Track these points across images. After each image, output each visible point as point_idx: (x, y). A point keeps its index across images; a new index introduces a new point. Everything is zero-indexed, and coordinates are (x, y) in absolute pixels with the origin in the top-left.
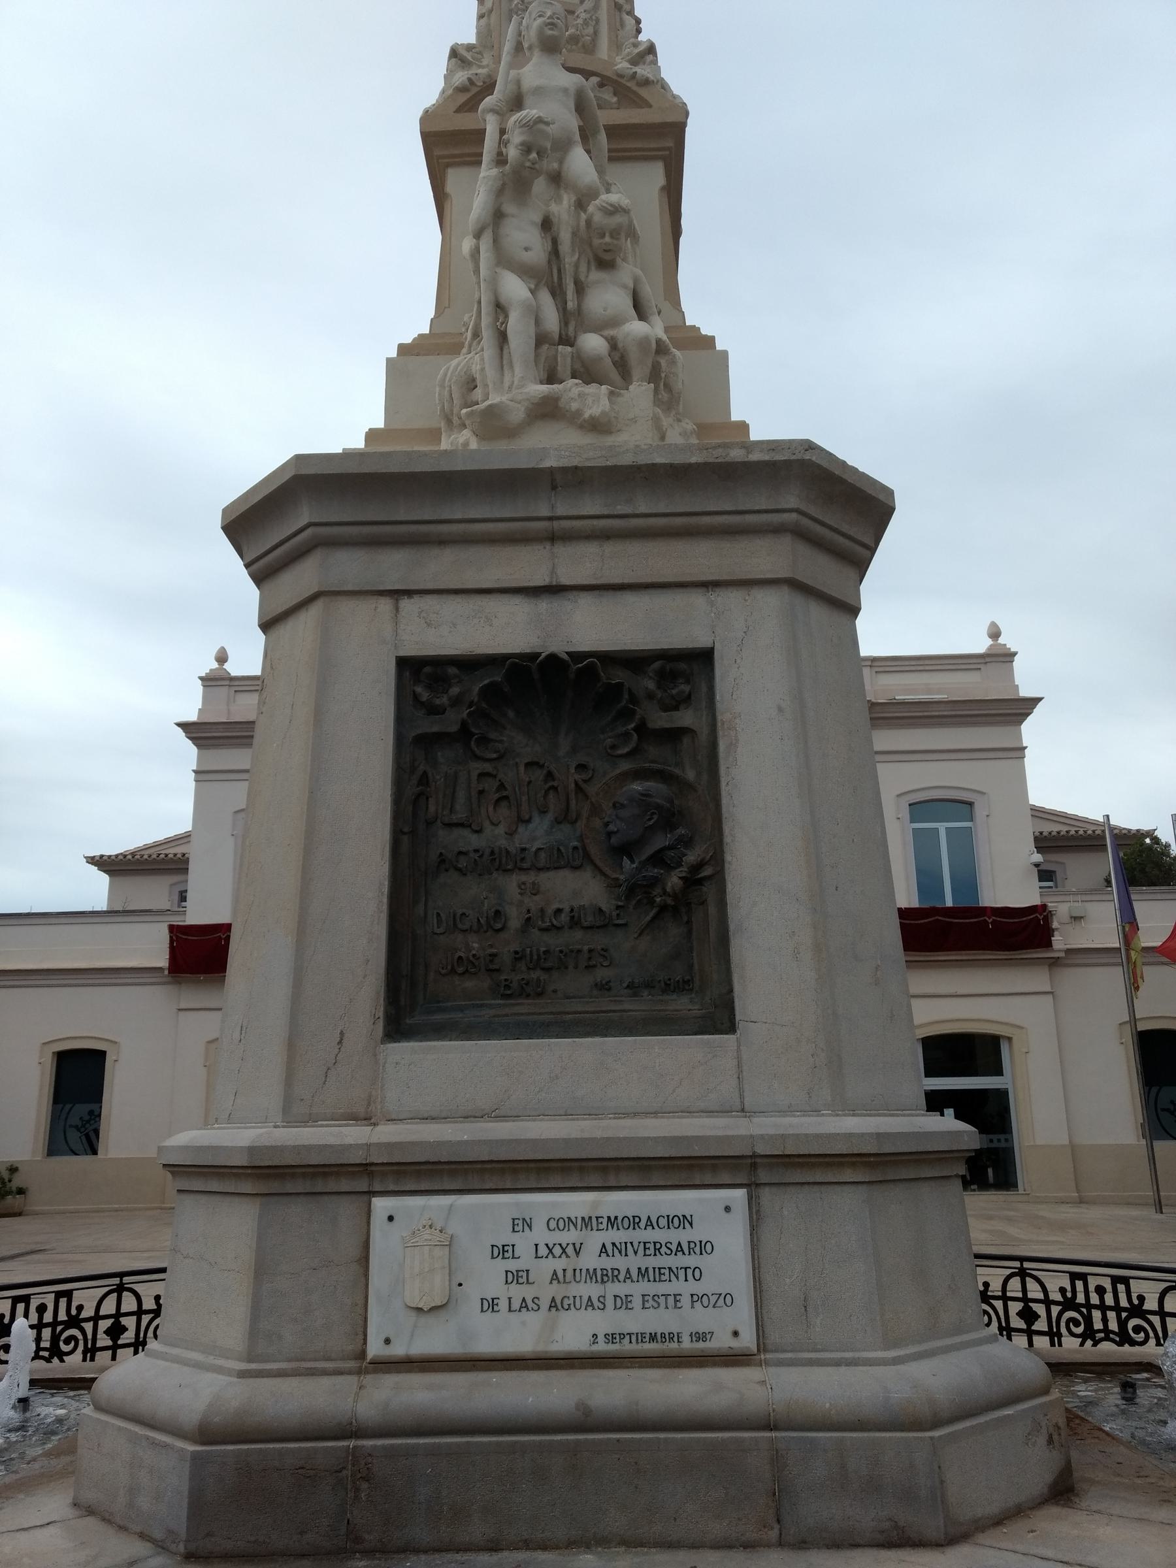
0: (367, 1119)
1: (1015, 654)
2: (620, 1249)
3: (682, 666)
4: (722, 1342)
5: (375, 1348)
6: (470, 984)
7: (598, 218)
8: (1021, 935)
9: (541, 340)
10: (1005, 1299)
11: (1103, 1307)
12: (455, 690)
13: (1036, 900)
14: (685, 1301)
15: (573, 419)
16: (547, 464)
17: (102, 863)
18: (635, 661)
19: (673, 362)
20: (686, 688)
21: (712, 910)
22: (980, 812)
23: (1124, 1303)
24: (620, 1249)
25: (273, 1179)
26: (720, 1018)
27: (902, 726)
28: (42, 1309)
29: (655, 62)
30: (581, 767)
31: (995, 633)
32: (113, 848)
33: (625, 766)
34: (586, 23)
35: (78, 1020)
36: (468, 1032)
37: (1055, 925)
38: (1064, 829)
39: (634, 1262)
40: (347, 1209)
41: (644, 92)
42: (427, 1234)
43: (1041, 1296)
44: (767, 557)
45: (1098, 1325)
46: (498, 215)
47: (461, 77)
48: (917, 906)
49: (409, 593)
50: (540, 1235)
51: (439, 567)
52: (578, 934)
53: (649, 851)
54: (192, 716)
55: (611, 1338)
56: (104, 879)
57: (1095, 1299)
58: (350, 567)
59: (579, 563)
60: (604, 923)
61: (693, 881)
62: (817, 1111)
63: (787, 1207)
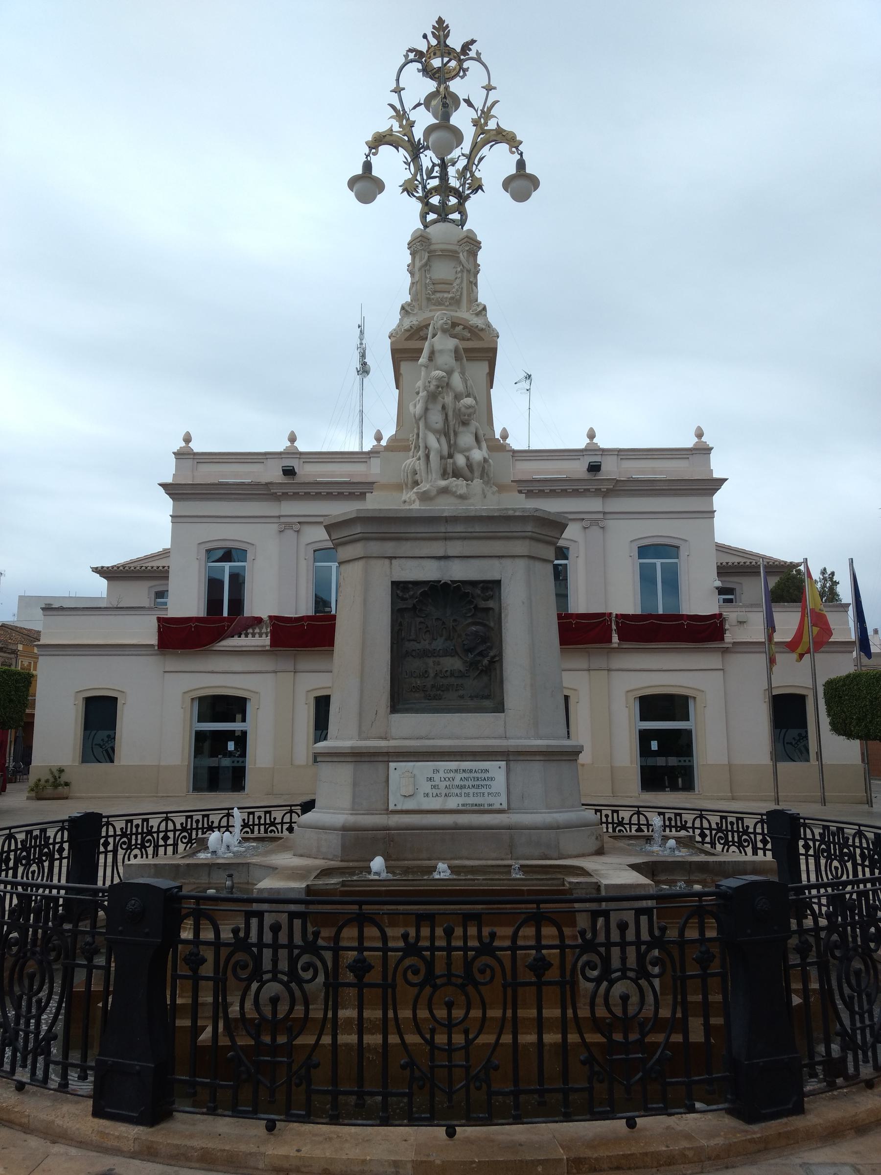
0: (386, 739)
1: (712, 449)
2: (467, 779)
3: (490, 585)
4: (497, 806)
5: (391, 807)
6: (417, 695)
7: (463, 409)
8: (705, 632)
9: (442, 458)
10: (630, 824)
11: (733, 831)
12: (411, 593)
13: (716, 611)
14: (486, 794)
15: (454, 494)
16: (445, 515)
17: (102, 572)
18: (473, 583)
19: (490, 465)
20: (491, 593)
21: (498, 672)
22: (683, 553)
23: (616, 821)
24: (467, 779)
25: (358, 756)
26: (499, 708)
27: (633, 496)
28: (259, 818)
29: (486, 315)
30: (455, 620)
31: (700, 434)
32: (109, 562)
33: (470, 620)
34: (457, 290)
35: (100, 677)
36: (417, 711)
37: (727, 627)
38: (742, 560)
39: (470, 783)
40: (381, 766)
41: (481, 334)
42: (407, 774)
43: (811, 837)
44: (520, 547)
45: (730, 839)
46: (426, 410)
47: (407, 324)
48: (639, 612)
49: (395, 558)
50: (442, 774)
51: (406, 548)
52: (453, 679)
53: (477, 651)
54: (169, 480)
55: (463, 805)
56: (105, 582)
57: (729, 827)
58: (375, 548)
59: (455, 548)
60: (462, 675)
61: (492, 662)
62: (529, 738)
63: (518, 767)
